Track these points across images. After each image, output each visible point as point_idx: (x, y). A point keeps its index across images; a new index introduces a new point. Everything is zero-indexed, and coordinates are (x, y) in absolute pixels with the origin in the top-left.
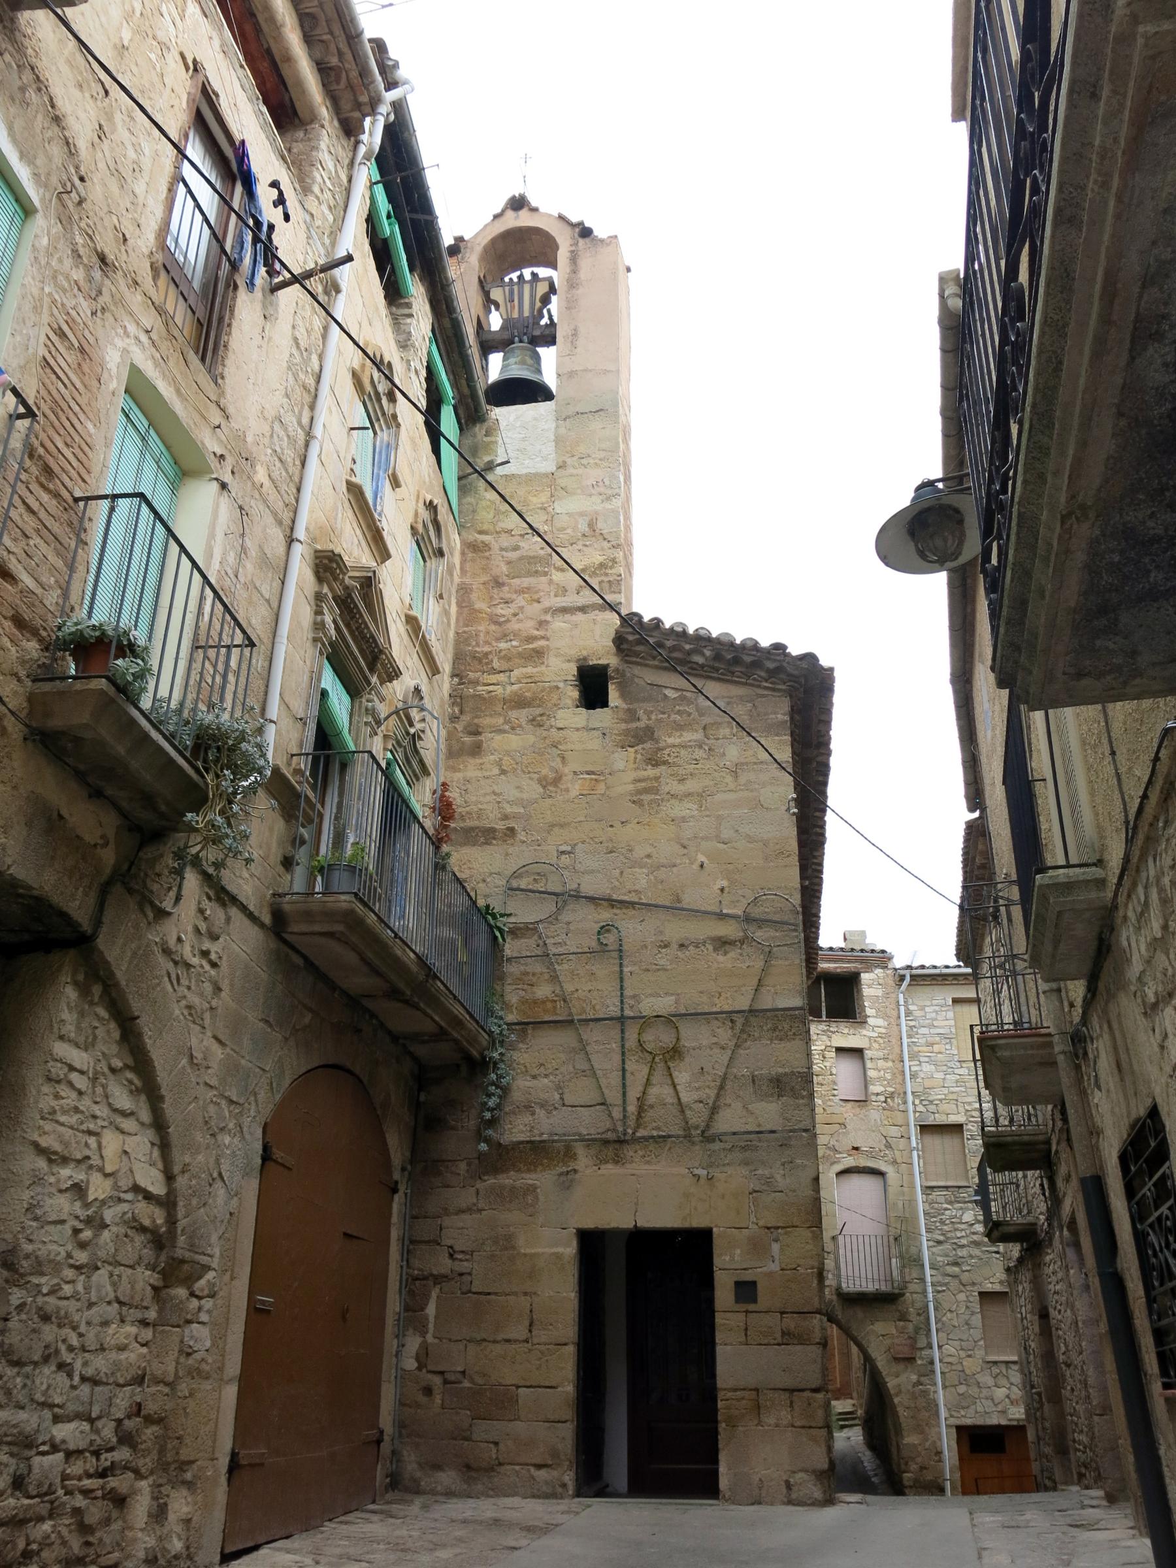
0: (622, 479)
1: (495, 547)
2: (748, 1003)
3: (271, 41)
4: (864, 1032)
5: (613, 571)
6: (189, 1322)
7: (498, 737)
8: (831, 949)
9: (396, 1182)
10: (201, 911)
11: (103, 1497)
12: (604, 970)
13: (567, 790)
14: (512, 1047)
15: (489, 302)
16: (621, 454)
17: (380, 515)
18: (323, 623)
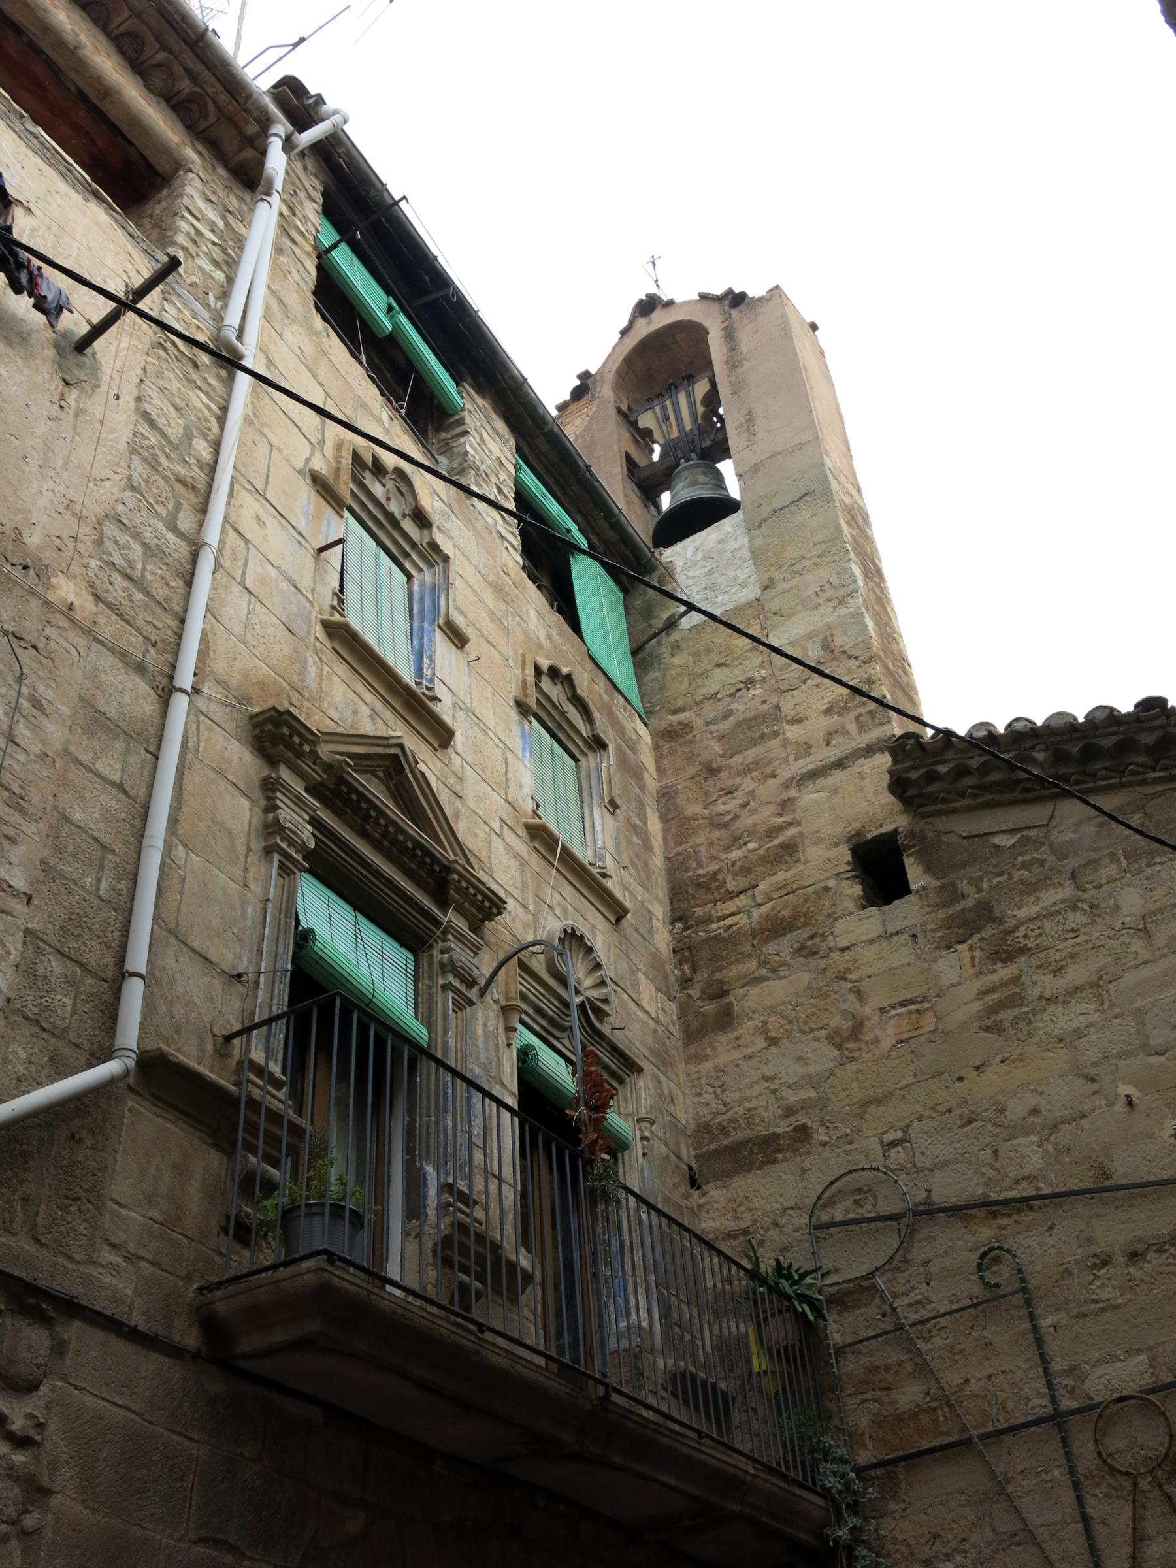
1: (698, 722)
7: (754, 991)
13: (876, 1041)
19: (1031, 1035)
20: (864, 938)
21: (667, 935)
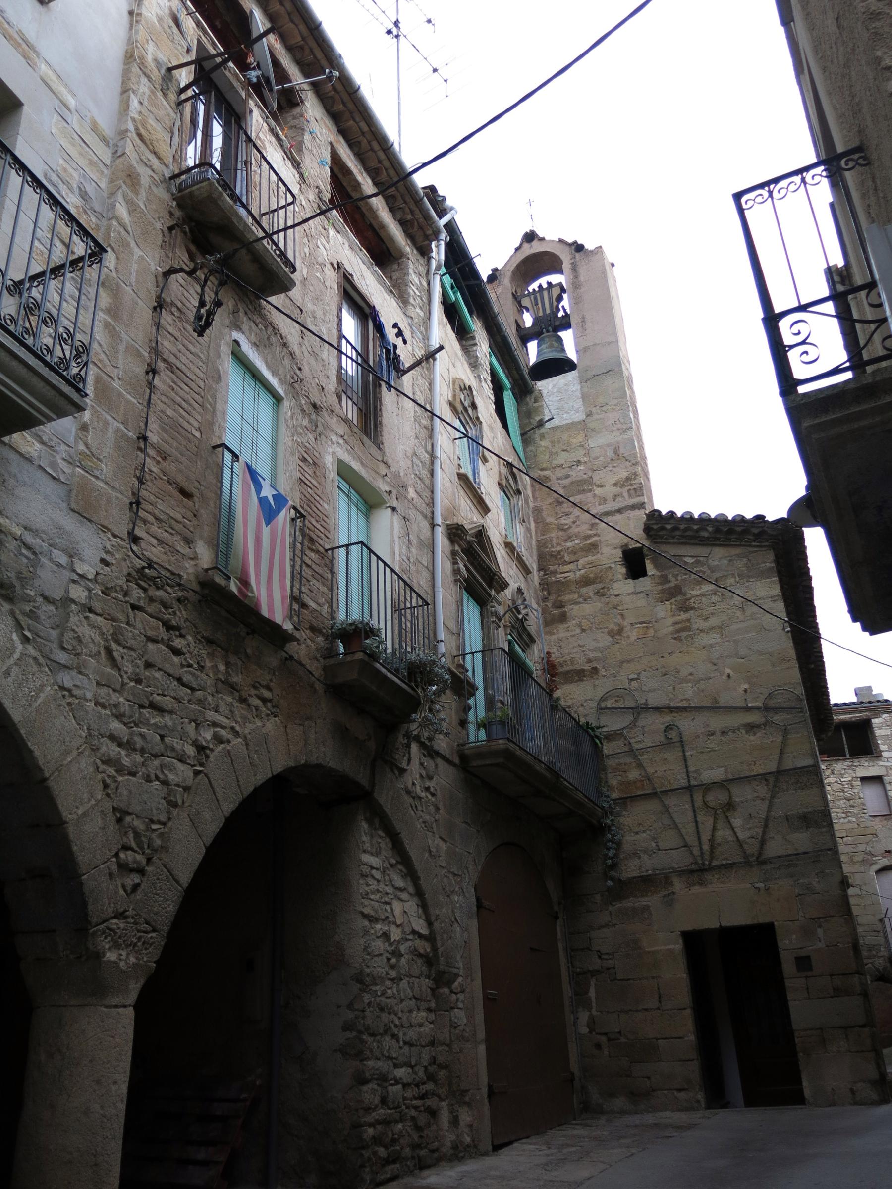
0: (632, 416)
1: (553, 477)
2: (776, 766)
3: (372, 220)
4: (881, 763)
5: (636, 481)
6: (453, 1008)
7: (576, 607)
8: (845, 704)
9: (557, 912)
10: (422, 764)
11: (425, 1111)
12: (673, 755)
13: (628, 637)
14: (619, 815)
15: (521, 308)
16: (629, 398)
17: (479, 484)
18: (459, 569)
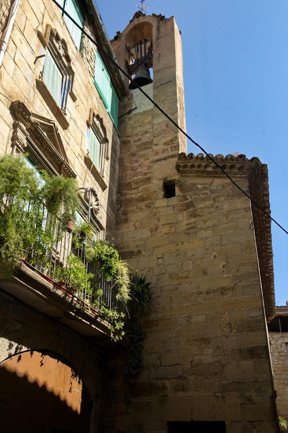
1: (132, 141)
13: (160, 232)
19: (196, 237)
20: (162, 206)
21: (116, 196)
